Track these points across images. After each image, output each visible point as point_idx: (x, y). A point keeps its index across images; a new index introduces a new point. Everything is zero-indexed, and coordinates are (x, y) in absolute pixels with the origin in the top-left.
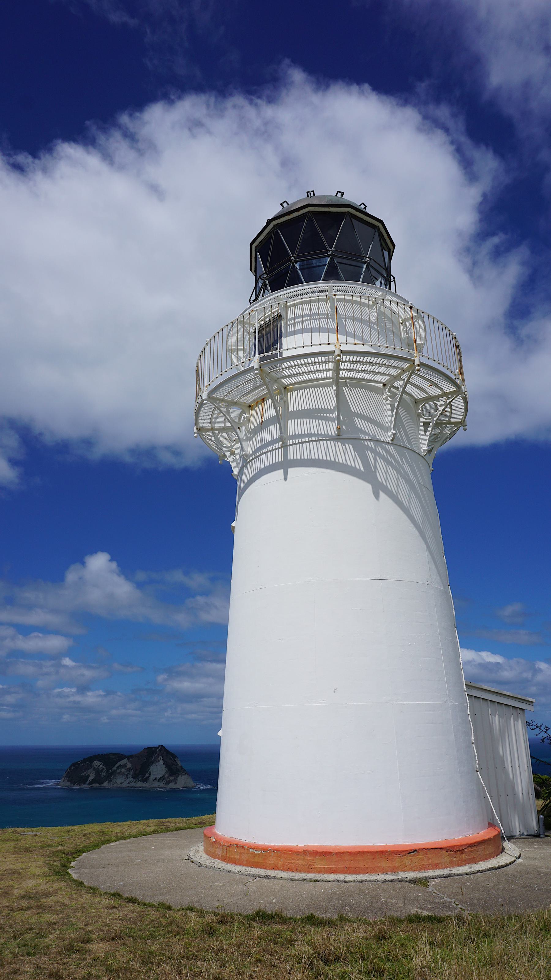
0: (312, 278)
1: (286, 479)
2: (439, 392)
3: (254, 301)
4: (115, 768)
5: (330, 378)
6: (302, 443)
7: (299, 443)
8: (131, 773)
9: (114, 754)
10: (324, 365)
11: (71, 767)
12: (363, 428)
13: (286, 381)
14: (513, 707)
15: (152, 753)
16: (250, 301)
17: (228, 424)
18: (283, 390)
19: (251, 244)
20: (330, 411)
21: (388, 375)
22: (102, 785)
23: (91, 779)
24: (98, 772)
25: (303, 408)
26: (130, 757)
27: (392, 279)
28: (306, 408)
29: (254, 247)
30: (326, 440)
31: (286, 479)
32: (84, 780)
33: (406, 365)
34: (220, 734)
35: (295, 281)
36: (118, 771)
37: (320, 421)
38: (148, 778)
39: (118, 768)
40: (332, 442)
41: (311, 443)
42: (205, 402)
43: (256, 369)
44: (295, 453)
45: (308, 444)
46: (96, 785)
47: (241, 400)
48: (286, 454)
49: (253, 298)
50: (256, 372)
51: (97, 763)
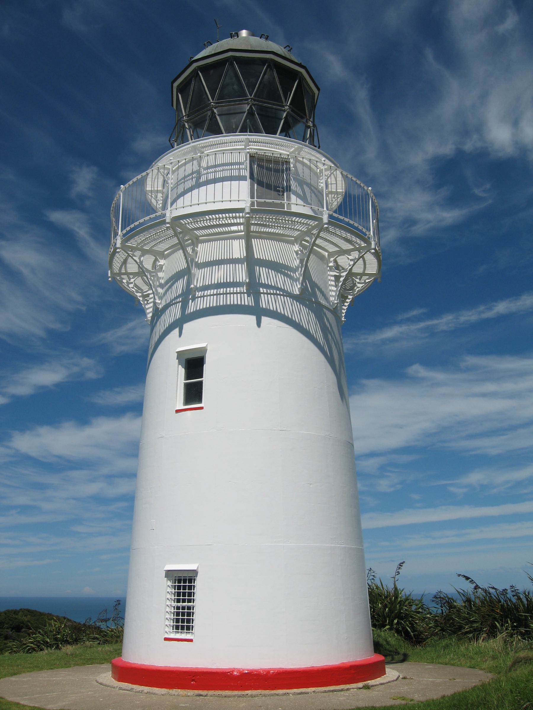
0: (231, 130)
1: (259, 324)
5: (241, 231)
6: (226, 294)
7: (223, 294)
12: (294, 318)
18: (194, 240)
20: (294, 270)
21: (298, 230)
25: (228, 258)
28: (228, 258)
29: (176, 85)
30: (284, 296)
31: (259, 324)
33: (312, 223)
35: (215, 130)
37: (270, 271)
40: (285, 298)
41: (235, 295)
42: (118, 250)
43: (168, 223)
44: (265, 301)
45: (232, 295)
47: (155, 248)
48: (257, 300)
50: (168, 225)
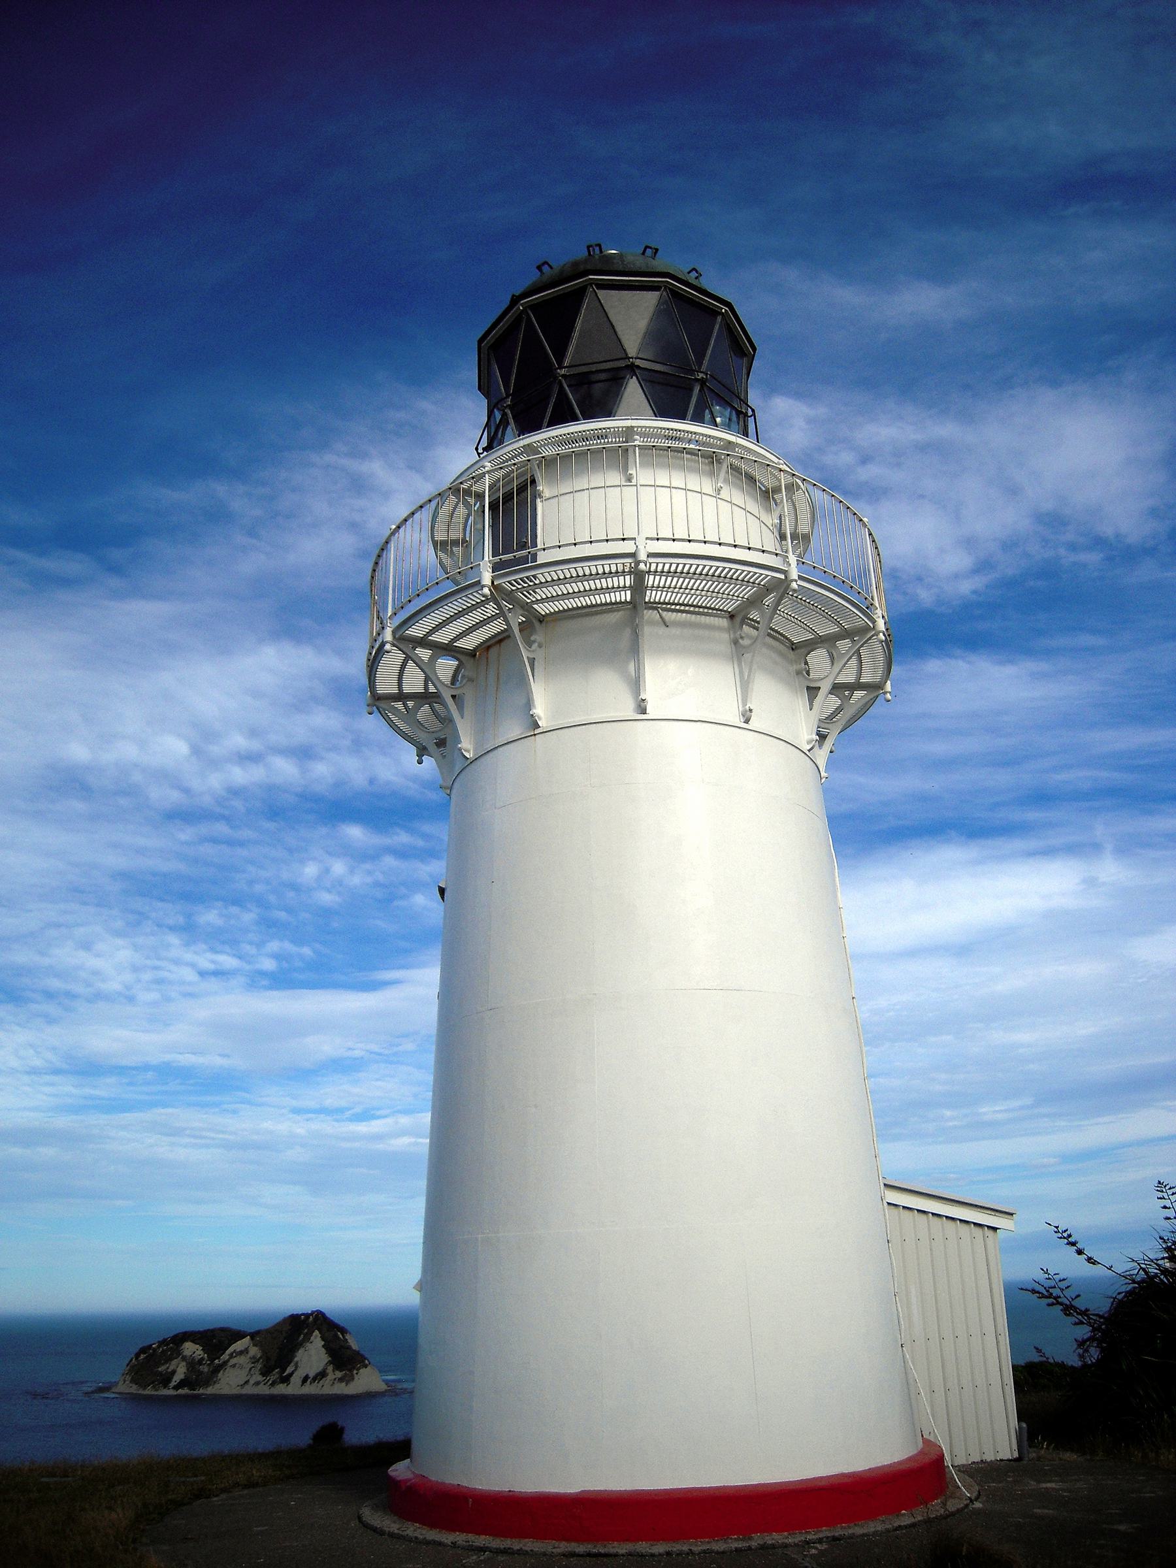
2: (835, 629)
3: (484, 449)
4: (225, 1357)
8: (259, 1366)
9: (222, 1330)
10: (609, 580)
11: (137, 1355)
13: (542, 609)
14: (975, 1224)
15: (298, 1328)
16: (477, 449)
17: (432, 689)
19: (480, 342)
22: (413, 1140)
23: (177, 1378)
24: (193, 1364)
26: (253, 1336)
27: (750, 413)
32: (166, 1380)
34: (311, 1442)
36: (233, 1361)
38: (291, 1375)
39: (231, 1356)
46: (184, 1391)
49: (484, 443)
51: (189, 1348)
